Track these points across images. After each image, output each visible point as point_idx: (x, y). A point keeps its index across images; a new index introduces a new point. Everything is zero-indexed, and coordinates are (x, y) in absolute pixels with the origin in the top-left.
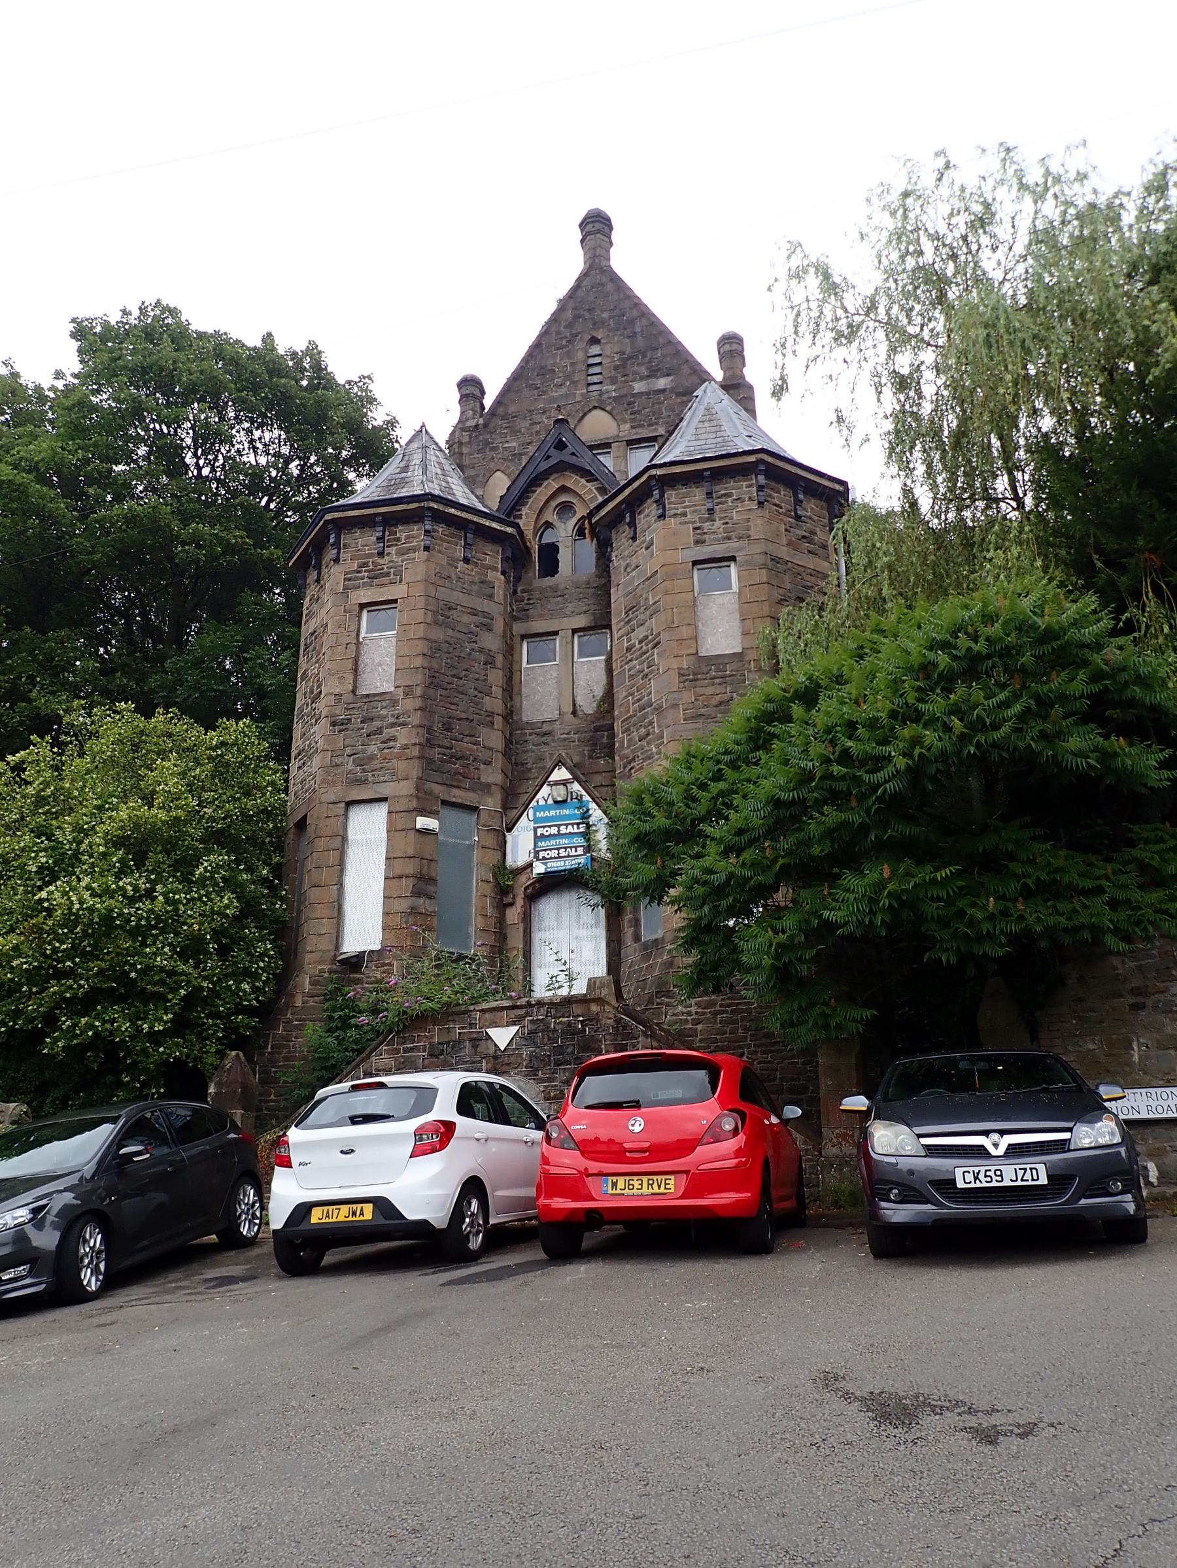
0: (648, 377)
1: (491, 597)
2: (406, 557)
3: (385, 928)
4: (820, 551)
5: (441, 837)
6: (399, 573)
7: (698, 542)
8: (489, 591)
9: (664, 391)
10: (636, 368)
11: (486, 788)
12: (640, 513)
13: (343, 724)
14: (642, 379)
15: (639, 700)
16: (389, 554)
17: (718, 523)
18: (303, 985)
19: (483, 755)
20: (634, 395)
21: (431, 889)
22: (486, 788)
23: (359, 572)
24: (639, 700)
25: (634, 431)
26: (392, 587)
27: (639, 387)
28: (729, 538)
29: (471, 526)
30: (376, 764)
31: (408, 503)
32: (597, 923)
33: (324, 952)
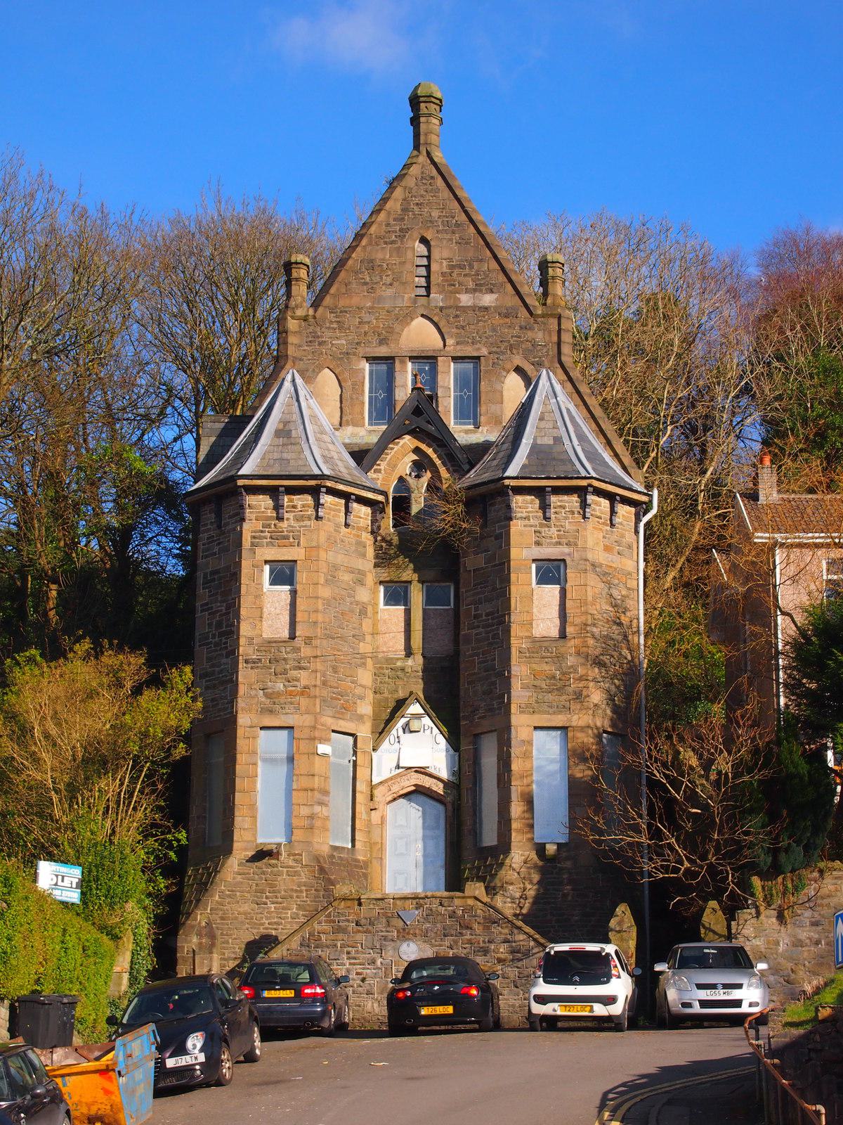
0: (475, 290)
1: (364, 555)
2: (302, 524)
3: (424, 828)
4: (626, 551)
5: (331, 758)
6: (297, 538)
7: (538, 544)
8: (361, 549)
9: (486, 309)
10: (461, 279)
11: (360, 718)
12: (492, 505)
13: (254, 663)
14: (467, 291)
15: (484, 662)
16: (288, 519)
17: (554, 530)
18: (232, 866)
19: (358, 691)
20: (458, 308)
21: (325, 798)
22: (360, 718)
23: (262, 532)
24: (484, 662)
25: (459, 347)
26: (290, 549)
27: (465, 299)
28: (559, 543)
29: (353, 497)
30: (282, 699)
31: (306, 480)
32: (437, 827)
33: (248, 842)
